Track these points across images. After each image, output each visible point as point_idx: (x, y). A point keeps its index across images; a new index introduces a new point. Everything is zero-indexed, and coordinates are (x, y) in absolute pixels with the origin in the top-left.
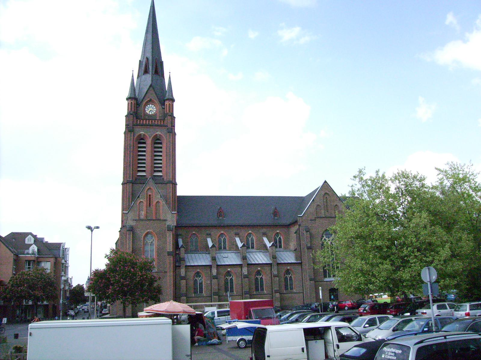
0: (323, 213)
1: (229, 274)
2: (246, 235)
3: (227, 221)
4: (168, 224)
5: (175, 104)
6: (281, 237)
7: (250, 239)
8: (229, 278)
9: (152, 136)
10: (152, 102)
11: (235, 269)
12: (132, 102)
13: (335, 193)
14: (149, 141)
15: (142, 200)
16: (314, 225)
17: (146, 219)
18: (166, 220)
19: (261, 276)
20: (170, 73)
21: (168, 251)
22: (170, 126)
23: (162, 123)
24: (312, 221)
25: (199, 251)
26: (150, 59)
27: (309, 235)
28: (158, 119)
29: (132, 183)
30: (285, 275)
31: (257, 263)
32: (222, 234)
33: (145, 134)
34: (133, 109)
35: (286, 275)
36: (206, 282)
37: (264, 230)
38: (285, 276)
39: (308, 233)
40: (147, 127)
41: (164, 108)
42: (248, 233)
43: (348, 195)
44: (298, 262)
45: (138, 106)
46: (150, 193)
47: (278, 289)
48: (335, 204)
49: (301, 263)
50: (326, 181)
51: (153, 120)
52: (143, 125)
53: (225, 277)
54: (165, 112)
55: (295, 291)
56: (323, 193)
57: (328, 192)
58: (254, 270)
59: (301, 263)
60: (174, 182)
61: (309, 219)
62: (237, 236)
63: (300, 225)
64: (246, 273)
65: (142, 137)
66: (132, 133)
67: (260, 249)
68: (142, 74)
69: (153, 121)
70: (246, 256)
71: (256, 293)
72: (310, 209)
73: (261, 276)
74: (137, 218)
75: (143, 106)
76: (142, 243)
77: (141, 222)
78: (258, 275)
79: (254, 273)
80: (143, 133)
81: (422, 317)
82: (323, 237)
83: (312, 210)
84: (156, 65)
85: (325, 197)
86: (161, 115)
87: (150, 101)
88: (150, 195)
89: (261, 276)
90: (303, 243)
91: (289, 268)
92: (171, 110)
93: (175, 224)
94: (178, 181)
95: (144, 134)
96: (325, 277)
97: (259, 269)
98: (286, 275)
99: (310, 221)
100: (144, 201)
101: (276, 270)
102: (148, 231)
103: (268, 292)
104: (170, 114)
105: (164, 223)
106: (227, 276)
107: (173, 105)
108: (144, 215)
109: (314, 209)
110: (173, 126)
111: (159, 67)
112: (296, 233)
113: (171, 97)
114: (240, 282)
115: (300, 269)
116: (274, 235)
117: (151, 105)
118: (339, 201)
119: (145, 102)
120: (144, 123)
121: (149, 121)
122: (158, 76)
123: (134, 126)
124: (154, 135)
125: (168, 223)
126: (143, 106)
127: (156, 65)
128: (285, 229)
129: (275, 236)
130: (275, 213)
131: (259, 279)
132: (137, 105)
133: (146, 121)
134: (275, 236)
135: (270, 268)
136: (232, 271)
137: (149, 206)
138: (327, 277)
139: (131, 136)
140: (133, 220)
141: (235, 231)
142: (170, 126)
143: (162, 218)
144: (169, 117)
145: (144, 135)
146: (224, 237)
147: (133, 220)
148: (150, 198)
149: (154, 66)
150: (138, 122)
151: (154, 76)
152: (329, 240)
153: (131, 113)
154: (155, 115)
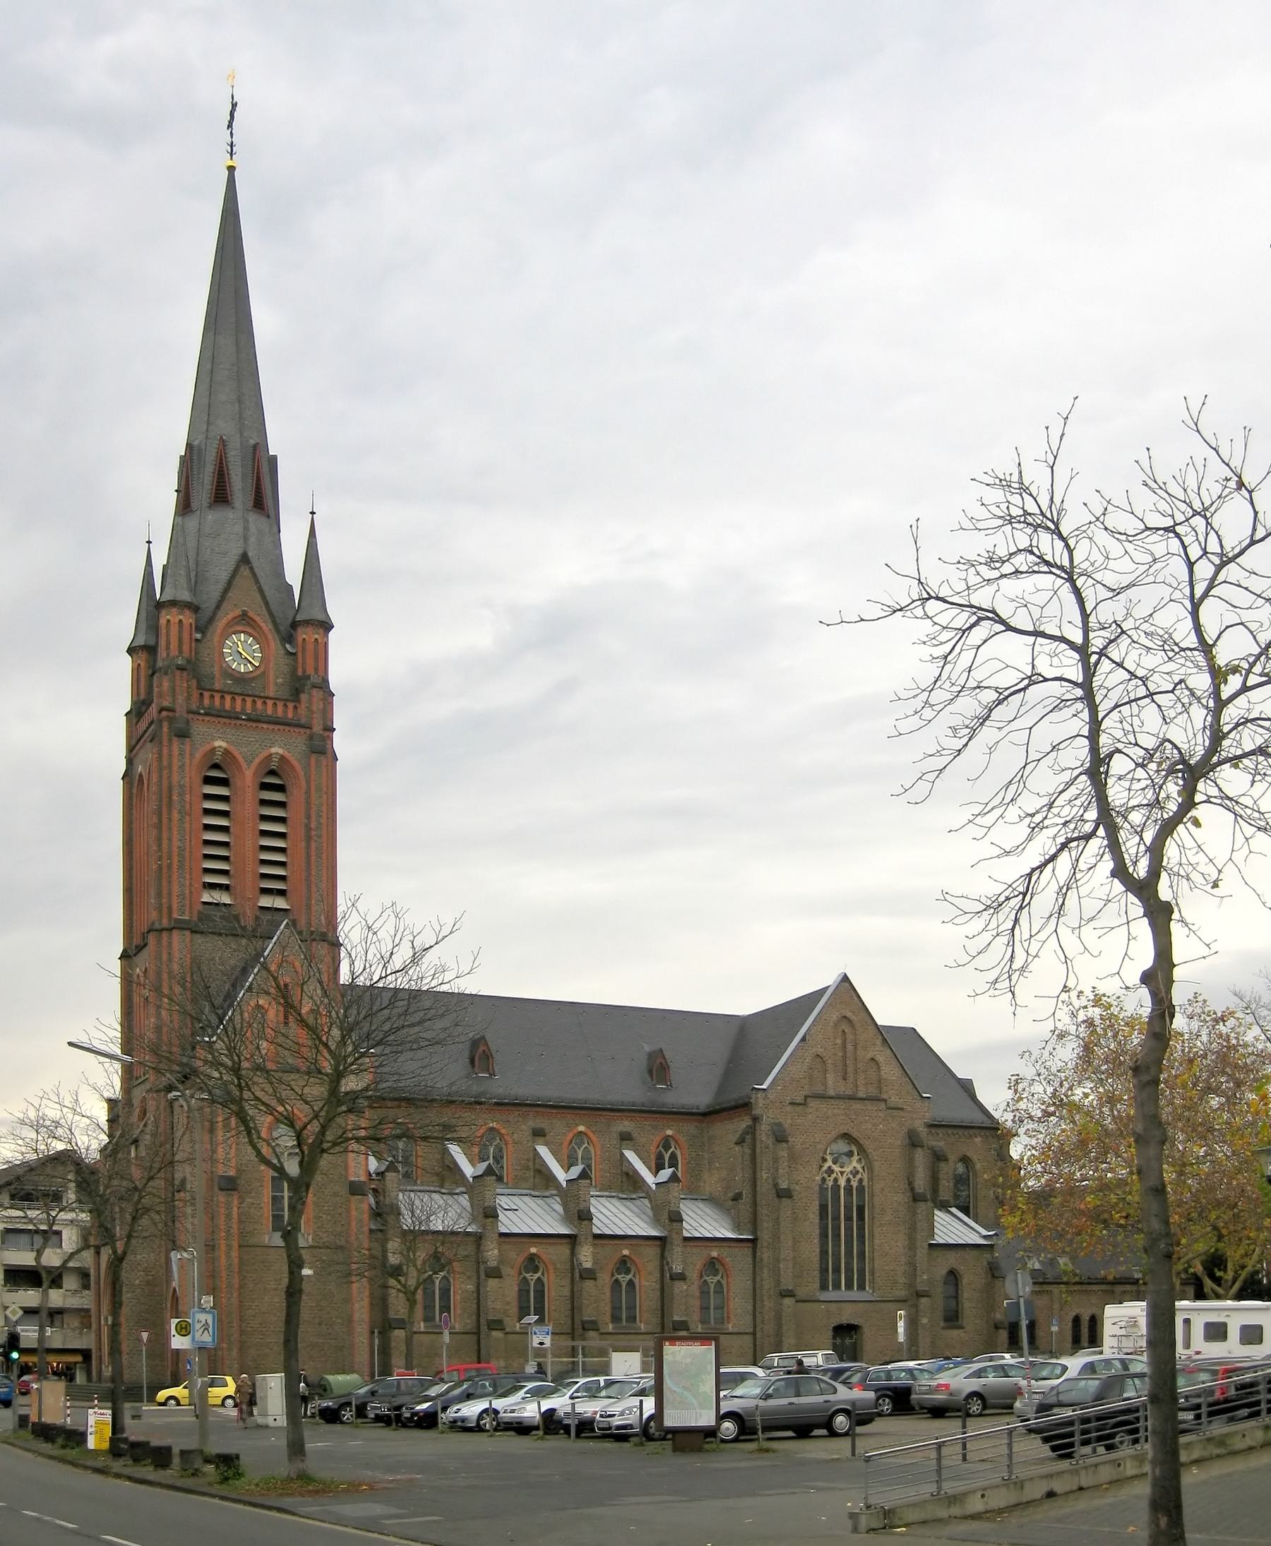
0: (833, 1084)
1: (532, 1263)
2: (569, 1138)
3: (502, 1085)
6: (678, 1153)
7: (580, 1153)
8: (532, 1277)
9: (257, 761)
10: (248, 624)
11: (551, 1249)
14: (247, 778)
19: (537, 1275)
21: (353, 1179)
22: (317, 729)
23: (290, 715)
25: (415, 1184)
30: (613, 1275)
31: (698, 1235)
32: (492, 1129)
33: (286, 754)
36: (463, 1286)
37: (626, 1125)
38: (614, 1278)
42: (575, 1132)
48: (869, 1056)
50: (848, 975)
53: (613, 1275)
54: (300, 673)
57: (849, 1014)
58: (612, 1253)
59: (753, 1242)
62: (541, 1139)
64: (588, 1265)
65: (217, 758)
67: (609, 1188)
68: (205, 504)
69: (259, 703)
71: (613, 1328)
73: (718, 1278)
75: (216, 639)
78: (619, 1271)
80: (224, 745)
82: (824, 1160)
85: (840, 1030)
89: (537, 1275)
91: (715, 1254)
95: (225, 749)
96: (824, 1287)
97: (626, 1252)
99: (789, 1108)
106: (619, 1274)
107: (326, 645)
109: (805, 1068)
111: (265, 470)
112: (740, 1142)
113: (321, 617)
114: (566, 1292)
115: (750, 1259)
118: (883, 1045)
119: (225, 621)
120: (238, 709)
121: (222, 697)
122: (264, 519)
124: (262, 756)
128: (691, 1128)
129: (658, 1147)
131: (624, 1285)
133: (254, 701)
134: (658, 1147)
135: (658, 1251)
136: (544, 1257)
138: (828, 1290)
141: (533, 1122)
142: (317, 729)
145: (226, 752)
146: (584, 1146)
150: (206, 702)
152: (842, 1173)
154: (259, 676)
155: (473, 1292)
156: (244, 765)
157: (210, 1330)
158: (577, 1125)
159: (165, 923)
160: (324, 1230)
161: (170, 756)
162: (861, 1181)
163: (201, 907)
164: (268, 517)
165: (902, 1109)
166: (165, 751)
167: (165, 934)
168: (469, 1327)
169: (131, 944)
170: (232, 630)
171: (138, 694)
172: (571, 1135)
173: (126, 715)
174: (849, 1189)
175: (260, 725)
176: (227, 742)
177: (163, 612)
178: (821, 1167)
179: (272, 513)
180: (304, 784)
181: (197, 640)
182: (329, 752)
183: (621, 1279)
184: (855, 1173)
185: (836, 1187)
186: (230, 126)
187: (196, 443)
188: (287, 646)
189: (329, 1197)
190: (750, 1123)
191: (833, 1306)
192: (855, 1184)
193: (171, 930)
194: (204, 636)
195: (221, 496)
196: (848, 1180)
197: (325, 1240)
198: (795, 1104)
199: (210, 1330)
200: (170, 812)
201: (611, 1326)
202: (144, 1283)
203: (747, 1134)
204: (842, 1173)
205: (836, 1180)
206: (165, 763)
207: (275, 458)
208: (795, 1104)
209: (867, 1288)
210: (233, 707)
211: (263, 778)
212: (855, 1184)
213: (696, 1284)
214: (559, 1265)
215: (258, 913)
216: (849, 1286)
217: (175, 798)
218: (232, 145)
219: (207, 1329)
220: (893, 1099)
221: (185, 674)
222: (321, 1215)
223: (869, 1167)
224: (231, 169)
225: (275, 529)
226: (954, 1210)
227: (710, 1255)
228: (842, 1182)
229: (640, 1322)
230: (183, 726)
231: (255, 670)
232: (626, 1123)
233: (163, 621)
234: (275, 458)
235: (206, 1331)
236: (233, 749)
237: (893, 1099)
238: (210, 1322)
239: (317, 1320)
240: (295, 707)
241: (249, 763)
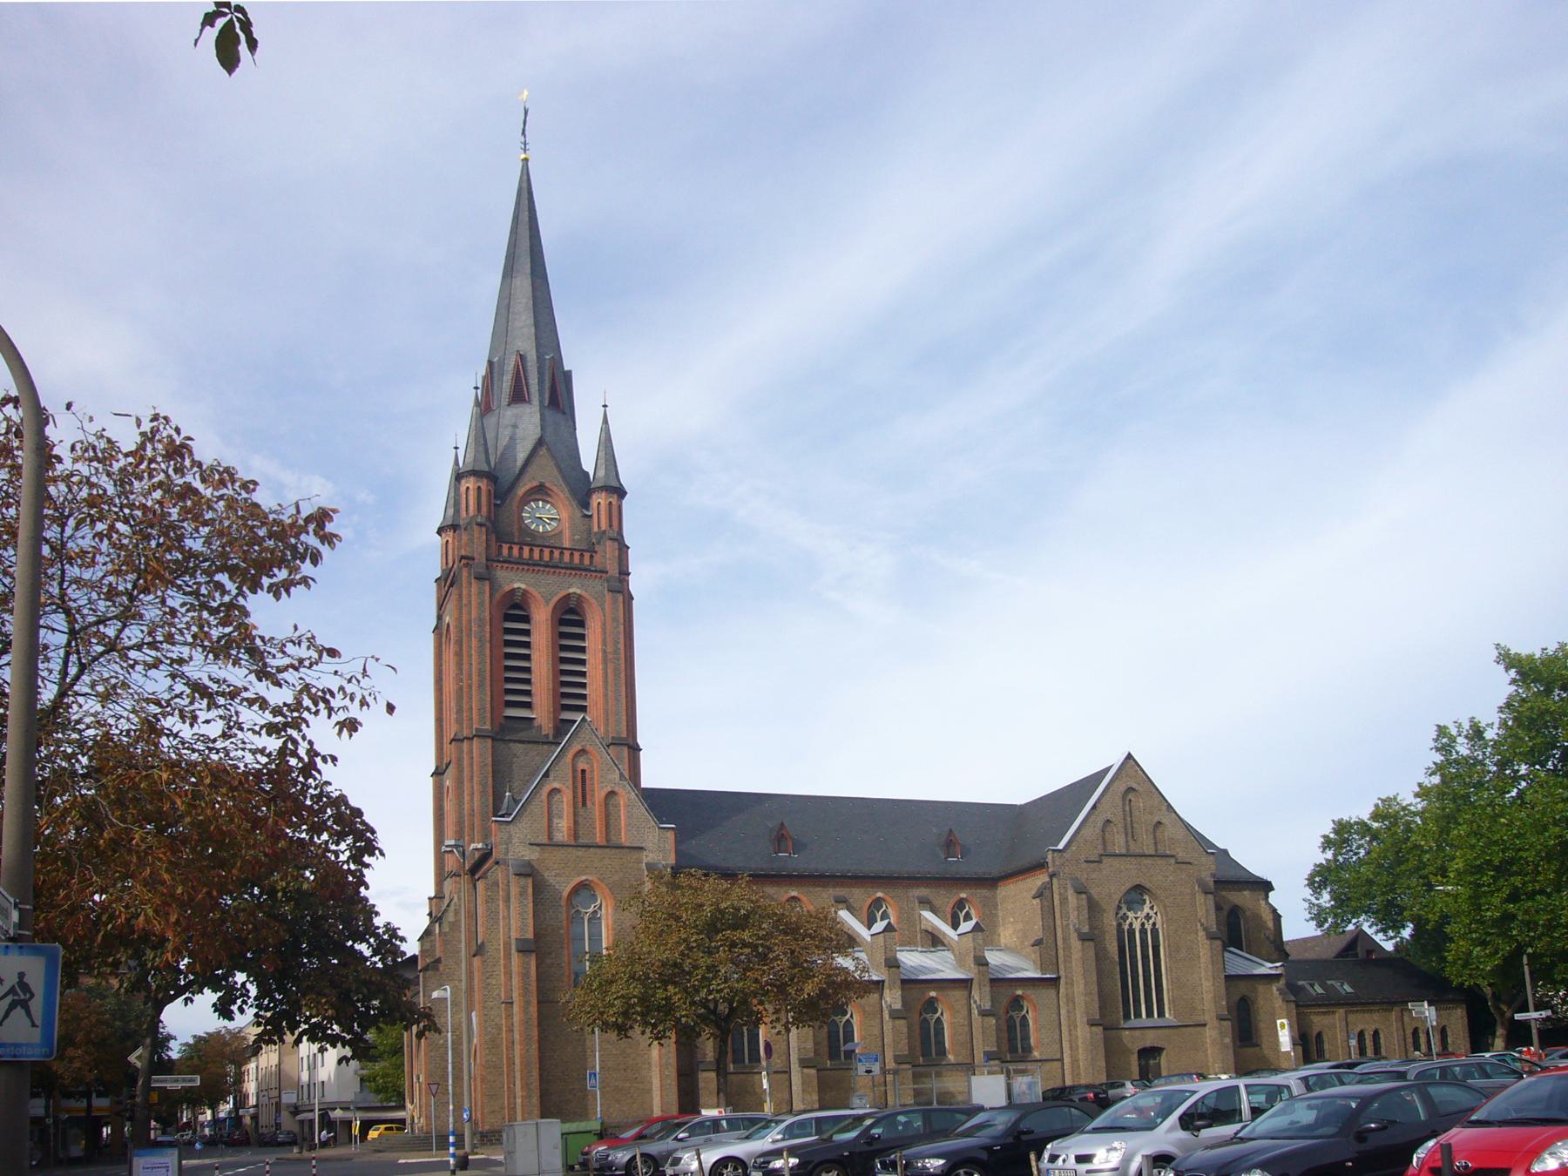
4: (650, 859)
5: (625, 502)
9: (555, 599)
12: (479, 488)
13: (1157, 789)
15: (556, 785)
16: (1094, 876)
17: (573, 843)
18: (642, 848)
20: (605, 406)
22: (613, 571)
23: (587, 561)
24: (1092, 865)
26: (532, 357)
27: (1084, 903)
28: (567, 544)
29: (494, 739)
30: (1008, 1013)
32: (793, 898)
33: (584, 593)
34: (484, 509)
35: (1011, 1013)
37: (923, 892)
39: (1084, 896)
40: (536, 568)
41: (591, 516)
43: (378, 921)
44: (1048, 976)
45: (499, 502)
46: (581, 765)
47: (995, 1049)
48: (1156, 819)
49: (1054, 982)
51: (556, 548)
52: (520, 562)
53: (921, 1014)
55: (1036, 1054)
56: (1123, 788)
57: (1134, 786)
60: (631, 744)
61: (1083, 858)
63: (1052, 876)
65: (518, 599)
66: (487, 583)
70: (896, 960)
72: (1085, 832)
74: (545, 840)
75: (515, 504)
76: (565, 915)
77: (560, 854)
79: (919, 1007)
81: (479, 1103)
83: (1091, 832)
84: (553, 375)
86: (577, 537)
87: (541, 492)
88: (583, 771)
90: (1065, 923)
92: (615, 524)
93: (672, 860)
94: (641, 740)
95: (524, 590)
98: (1011, 1013)
100: (564, 788)
101: (988, 997)
102: (583, 878)
103: (961, 1059)
104: (615, 535)
105: (635, 855)
108: (565, 829)
110: (624, 573)
111: (561, 388)
113: (614, 484)
116: (951, 905)
117: (540, 503)
123: (490, 563)
125: (649, 857)
126: (515, 504)
127: (553, 375)
130: (950, 844)
132: (495, 497)
137: (580, 804)
139: (481, 593)
140: (530, 844)
143: (624, 839)
144: (609, 543)
145: (525, 592)
147: (530, 844)
148: (582, 781)
149: (547, 385)
150: (505, 552)
151: (548, 413)
152: (1136, 918)
153: (479, 520)
157: (37, 1005)
159: (466, 733)
161: (470, 595)
162: (1154, 924)
163: (502, 721)
164: (564, 413)
165: (1190, 863)
166: (465, 592)
167: (465, 744)
169: (442, 763)
170: (532, 497)
171: (447, 563)
172: (870, 901)
173: (436, 581)
174: (1143, 931)
177: (463, 482)
178: (1117, 914)
179: (567, 410)
181: (496, 505)
182: (626, 591)
183: (929, 1019)
184: (1148, 917)
185: (1131, 932)
186: (524, 133)
187: (496, 360)
190: (1047, 879)
191: (1137, 1033)
192: (1148, 927)
193: (470, 739)
194: (503, 503)
195: (519, 396)
196: (1143, 924)
198: (1090, 862)
199: (37, 1005)
200: (469, 641)
201: (921, 1059)
203: (1045, 889)
204: (1136, 918)
205: (1131, 924)
206: (464, 602)
207: (570, 372)
208: (1090, 862)
209: (1167, 1015)
210: (531, 557)
211: (563, 614)
212: (1148, 927)
213: (1003, 1018)
214: (867, 1009)
215: (560, 725)
216: (1150, 1014)
218: (525, 144)
219: (25, 1005)
220: (1180, 855)
221: (484, 529)
224: (526, 160)
225: (571, 423)
226: (1232, 949)
228: (1137, 926)
230: (481, 571)
231: (538, 500)
233: (463, 489)
234: (570, 372)
235: (19, 1011)
236: (531, 589)
237: (1180, 855)
238: (36, 980)
240: (592, 557)
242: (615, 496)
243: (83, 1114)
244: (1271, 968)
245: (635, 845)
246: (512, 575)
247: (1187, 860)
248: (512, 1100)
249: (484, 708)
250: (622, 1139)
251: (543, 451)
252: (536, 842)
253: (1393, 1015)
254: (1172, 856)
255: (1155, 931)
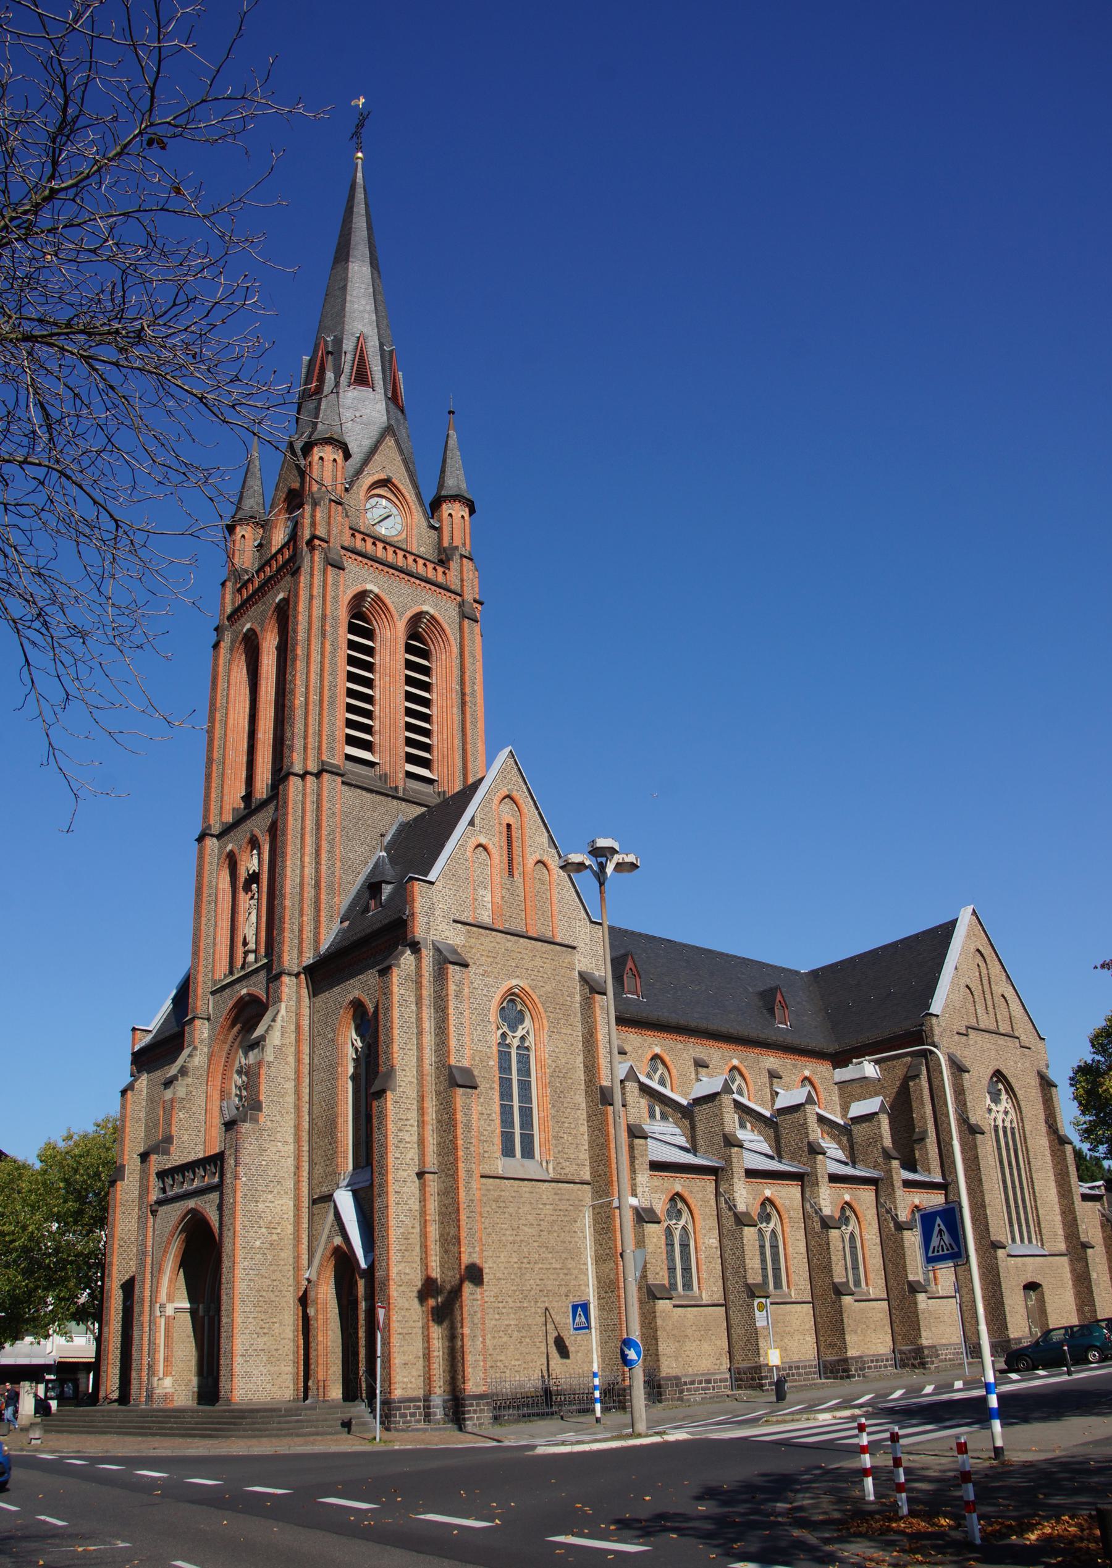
18: (574, 948)
99: (957, 1037)
102: (514, 982)
105: (566, 956)
147: (455, 921)
155: (716, 1248)
156: (396, 616)
158: (731, 1058)
160: (565, 1156)
168: (715, 1296)
175: (413, 580)
176: (379, 587)
180: (455, 650)
188: (431, 521)
189: (569, 1110)
197: (567, 1171)
202: (267, 1245)
217: (328, 628)
222: (561, 1134)
223: (1018, 1108)
227: (913, 1203)
229: (867, 1284)
232: (772, 1059)
239: (563, 1290)
241: (401, 615)
242: (467, 510)
243: (93, 1360)
244: (1089, 1188)
245: (567, 943)
246: (364, 572)
247: (1028, 1045)
248: (966, 1298)
249: (472, 723)
250: (902, 1389)
251: (390, 442)
252: (462, 919)
253: (34, 1384)
254: (1018, 1038)
255: (1012, 1129)
